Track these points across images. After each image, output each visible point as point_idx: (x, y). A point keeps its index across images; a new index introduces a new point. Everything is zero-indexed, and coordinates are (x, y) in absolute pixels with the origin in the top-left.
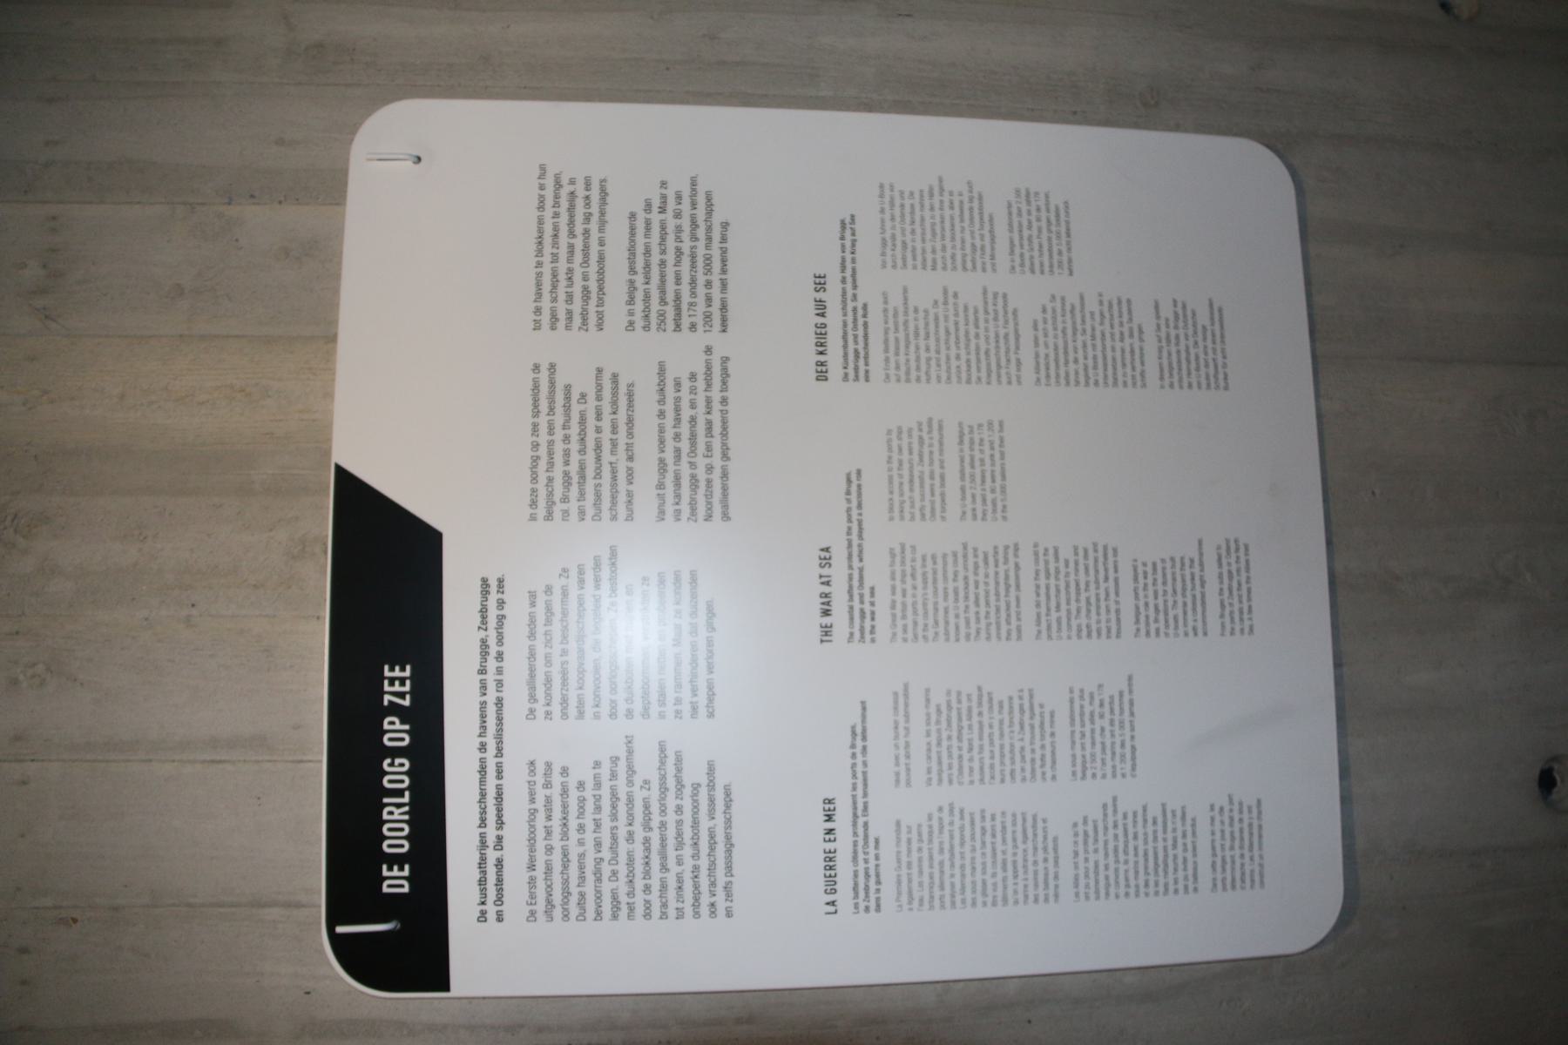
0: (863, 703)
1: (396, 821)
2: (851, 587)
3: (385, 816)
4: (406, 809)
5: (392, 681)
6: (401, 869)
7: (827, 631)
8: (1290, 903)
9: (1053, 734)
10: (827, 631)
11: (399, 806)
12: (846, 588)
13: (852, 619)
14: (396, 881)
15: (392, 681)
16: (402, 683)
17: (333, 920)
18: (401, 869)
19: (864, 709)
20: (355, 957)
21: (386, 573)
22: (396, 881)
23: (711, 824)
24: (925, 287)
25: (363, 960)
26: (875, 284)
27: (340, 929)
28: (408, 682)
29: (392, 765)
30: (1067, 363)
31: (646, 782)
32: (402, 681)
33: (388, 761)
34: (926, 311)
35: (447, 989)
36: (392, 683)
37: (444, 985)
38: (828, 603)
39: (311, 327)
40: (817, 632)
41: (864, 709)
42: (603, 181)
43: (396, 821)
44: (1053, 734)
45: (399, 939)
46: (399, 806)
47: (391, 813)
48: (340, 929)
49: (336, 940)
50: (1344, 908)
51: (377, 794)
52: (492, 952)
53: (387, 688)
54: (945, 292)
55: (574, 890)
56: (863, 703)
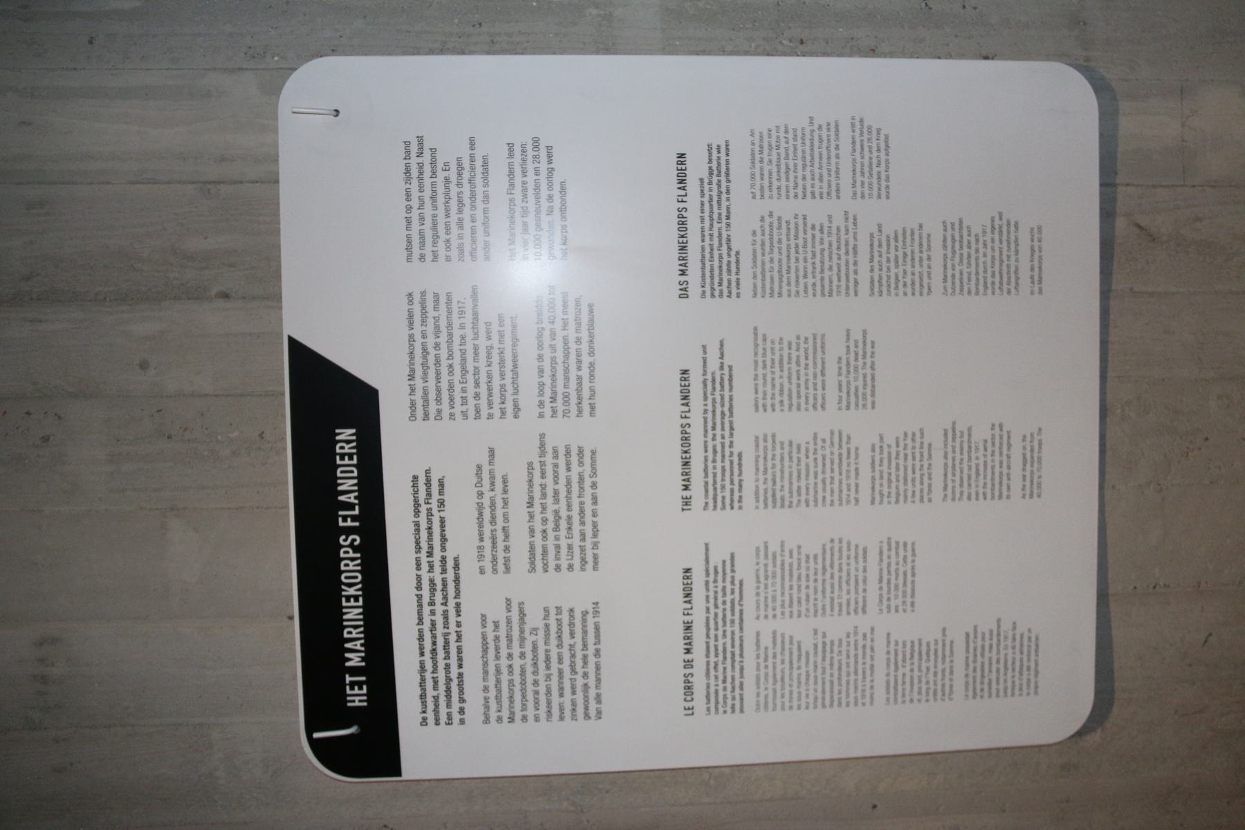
0: (707, 545)
1: (348, 484)
2: (703, 257)
3: (343, 568)
4: (354, 444)
5: (342, 457)
6: (361, 688)
7: (687, 502)
8: (1054, 704)
9: (865, 590)
10: (687, 502)
11: (355, 627)
12: (700, 257)
13: (707, 491)
14: (357, 698)
15: (342, 457)
16: (351, 458)
17: (309, 730)
18: (361, 688)
19: (707, 550)
20: (327, 753)
21: (331, 403)
22: (357, 698)
23: (581, 469)
24: (800, 629)
25: (334, 756)
26: (757, 627)
27: (316, 735)
28: (365, 687)
29: (345, 540)
30: (913, 284)
31: (536, 629)
32: (351, 457)
33: (343, 537)
34: (788, 222)
35: (399, 774)
36: (342, 458)
37: (397, 772)
38: (688, 480)
39: (274, 298)
40: (680, 502)
41: (707, 550)
42: (521, 604)
43: (350, 566)
44: (865, 590)
45: (361, 737)
46: (355, 627)
47: (350, 633)
48: (316, 735)
49: (314, 744)
50: (1098, 692)
51: (338, 647)
52: (424, 748)
53: (344, 604)
54: (815, 437)
55: (470, 367)
56: (707, 545)
